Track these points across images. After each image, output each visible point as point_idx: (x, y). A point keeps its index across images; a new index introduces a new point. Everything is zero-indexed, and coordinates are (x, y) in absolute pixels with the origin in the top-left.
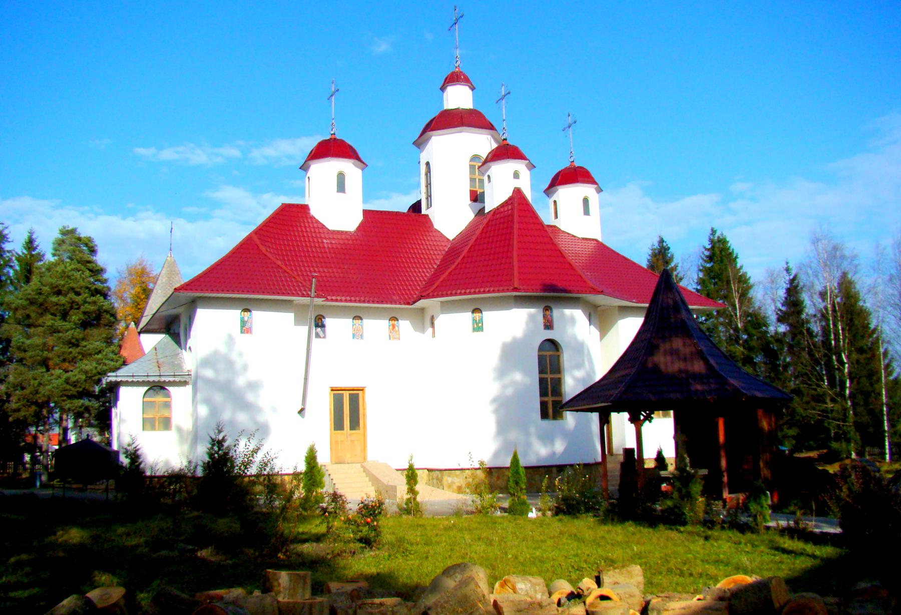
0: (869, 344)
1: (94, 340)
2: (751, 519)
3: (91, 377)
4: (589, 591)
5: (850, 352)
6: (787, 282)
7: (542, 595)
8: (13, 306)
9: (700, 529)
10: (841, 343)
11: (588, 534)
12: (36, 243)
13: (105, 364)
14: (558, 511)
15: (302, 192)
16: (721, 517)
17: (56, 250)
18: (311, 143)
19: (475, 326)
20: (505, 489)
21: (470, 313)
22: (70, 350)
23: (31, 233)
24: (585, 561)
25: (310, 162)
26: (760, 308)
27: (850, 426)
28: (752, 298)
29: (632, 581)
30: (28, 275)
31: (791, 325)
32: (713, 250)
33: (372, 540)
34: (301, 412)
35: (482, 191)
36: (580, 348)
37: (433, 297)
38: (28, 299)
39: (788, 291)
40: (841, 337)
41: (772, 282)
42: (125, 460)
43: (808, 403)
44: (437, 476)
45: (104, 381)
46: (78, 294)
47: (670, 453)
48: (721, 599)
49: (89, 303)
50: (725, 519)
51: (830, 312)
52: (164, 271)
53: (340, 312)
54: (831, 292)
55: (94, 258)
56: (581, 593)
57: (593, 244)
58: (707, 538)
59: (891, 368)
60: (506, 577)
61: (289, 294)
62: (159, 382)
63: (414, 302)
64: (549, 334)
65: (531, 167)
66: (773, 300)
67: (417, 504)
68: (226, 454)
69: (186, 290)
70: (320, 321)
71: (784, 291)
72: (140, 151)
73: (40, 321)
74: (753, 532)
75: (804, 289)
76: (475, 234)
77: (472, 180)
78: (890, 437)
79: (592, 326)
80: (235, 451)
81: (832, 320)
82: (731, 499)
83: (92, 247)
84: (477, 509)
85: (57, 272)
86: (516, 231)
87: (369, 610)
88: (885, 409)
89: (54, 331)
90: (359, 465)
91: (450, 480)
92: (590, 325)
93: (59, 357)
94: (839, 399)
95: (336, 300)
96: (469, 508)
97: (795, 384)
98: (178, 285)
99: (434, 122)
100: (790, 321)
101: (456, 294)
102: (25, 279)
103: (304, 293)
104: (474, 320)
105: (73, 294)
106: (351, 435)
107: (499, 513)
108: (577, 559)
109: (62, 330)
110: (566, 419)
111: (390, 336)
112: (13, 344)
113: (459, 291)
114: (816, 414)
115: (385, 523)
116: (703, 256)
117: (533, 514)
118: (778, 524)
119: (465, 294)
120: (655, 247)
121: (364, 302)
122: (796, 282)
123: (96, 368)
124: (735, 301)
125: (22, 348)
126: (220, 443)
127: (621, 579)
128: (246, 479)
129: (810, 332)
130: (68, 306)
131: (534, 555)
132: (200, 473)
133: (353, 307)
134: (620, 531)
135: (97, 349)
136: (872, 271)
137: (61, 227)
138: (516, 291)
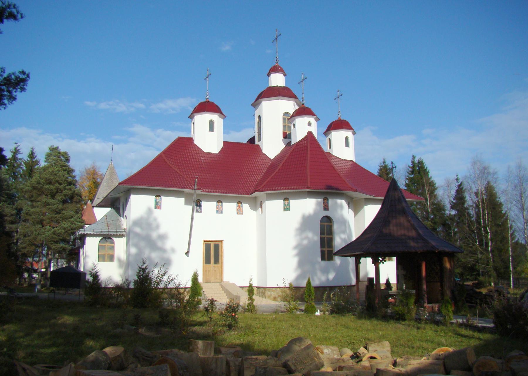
1: (69, 211)
2: (442, 318)
3: (67, 231)
4: (364, 354)
6: (457, 186)
7: (337, 356)
8: (24, 190)
9: (413, 323)
10: (487, 222)
11: (352, 325)
12: (35, 155)
13: (75, 225)
14: (332, 312)
15: (189, 130)
16: (426, 316)
17: (46, 158)
20: (302, 300)
21: (283, 200)
22: (56, 216)
24: (354, 339)
25: (195, 114)
27: (491, 268)
28: (436, 195)
29: (384, 349)
30: (31, 173)
31: (458, 210)
32: (414, 168)
33: (233, 325)
34: (187, 253)
35: (289, 132)
36: (344, 222)
37: (262, 191)
38: (33, 187)
39: (457, 191)
41: (448, 186)
42: (89, 277)
43: (467, 254)
45: (77, 233)
46: (60, 184)
47: (393, 281)
48: (437, 359)
50: (427, 318)
51: (481, 204)
52: (108, 172)
53: (209, 199)
54: (482, 192)
56: (359, 355)
57: (350, 163)
58: (418, 328)
60: (318, 346)
61: (182, 187)
62: (108, 234)
63: (251, 194)
64: (326, 213)
65: (317, 120)
66: (449, 197)
67: (254, 306)
68: (147, 276)
69: (125, 184)
70: (199, 203)
71: (455, 191)
72: (89, 103)
73: (39, 199)
74: (443, 325)
75: (466, 191)
76: (286, 156)
77: (284, 126)
78: (514, 274)
79: (350, 209)
80: (153, 274)
81: (482, 208)
82: (429, 307)
84: (287, 309)
85: (49, 171)
86: (309, 155)
87: (250, 362)
88: (511, 258)
89: (46, 204)
90: (219, 284)
91: (269, 293)
92: (349, 208)
93: (49, 219)
94: (485, 253)
95: (208, 192)
96: (283, 309)
97: (460, 243)
98: (121, 181)
99: (264, 93)
100: (458, 208)
101: (275, 190)
102: (29, 175)
103: (191, 187)
104: (285, 205)
105: (58, 184)
106: (214, 267)
107: (299, 312)
108: (349, 338)
109: (51, 204)
110: (335, 261)
111: (237, 212)
112: (24, 211)
113: (277, 188)
114: (472, 260)
115: (239, 316)
116: (408, 171)
117: (318, 314)
118: (457, 321)
119: (280, 189)
120: (382, 165)
121: (224, 193)
122: (462, 186)
123: (70, 226)
124: (427, 196)
127: (378, 348)
130: (55, 191)
131: (325, 336)
132: (132, 286)
133: (217, 195)
134: (369, 323)
135: (70, 215)
138: (309, 189)
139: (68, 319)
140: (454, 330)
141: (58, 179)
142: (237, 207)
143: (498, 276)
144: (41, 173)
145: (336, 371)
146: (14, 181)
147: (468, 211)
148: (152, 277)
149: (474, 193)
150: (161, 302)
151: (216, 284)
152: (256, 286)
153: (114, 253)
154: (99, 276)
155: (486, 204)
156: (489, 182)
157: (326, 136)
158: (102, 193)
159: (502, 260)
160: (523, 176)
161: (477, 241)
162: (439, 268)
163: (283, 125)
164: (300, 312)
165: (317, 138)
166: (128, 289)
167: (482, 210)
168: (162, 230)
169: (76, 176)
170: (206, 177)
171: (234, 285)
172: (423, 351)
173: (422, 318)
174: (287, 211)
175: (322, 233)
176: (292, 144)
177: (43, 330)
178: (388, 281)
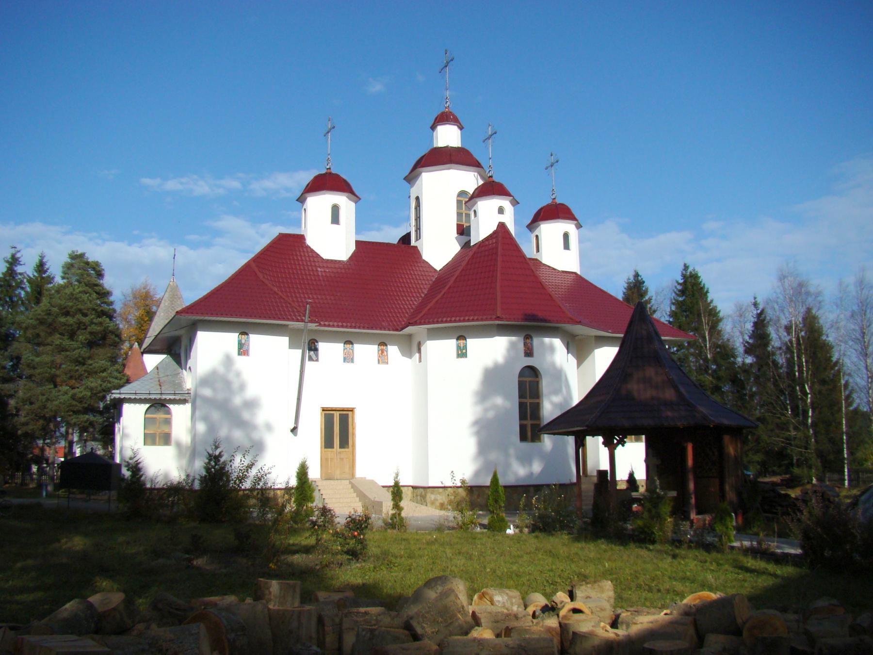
0: (831, 376)
1: (100, 360)
2: (716, 539)
3: (96, 394)
4: (563, 604)
5: (813, 383)
7: (518, 607)
8: (24, 325)
10: (805, 375)
11: (563, 551)
12: (47, 267)
13: (110, 382)
14: (534, 529)
15: (298, 223)
16: (689, 536)
17: (65, 273)
18: (308, 177)
19: (460, 352)
20: (484, 507)
22: (77, 368)
23: (42, 257)
24: (560, 576)
25: (307, 195)
26: (728, 340)
27: (812, 453)
29: (603, 595)
30: (39, 296)
31: (757, 357)
32: (686, 285)
33: (359, 552)
34: (294, 430)
35: (468, 225)
36: (559, 375)
37: (420, 324)
38: (38, 319)
40: (805, 369)
41: (741, 316)
42: (126, 473)
44: (422, 493)
45: (108, 398)
46: (85, 315)
47: (641, 475)
49: (96, 324)
50: (692, 538)
51: (795, 345)
53: (332, 337)
54: (796, 326)
55: (101, 281)
56: (555, 606)
57: (572, 277)
58: (674, 556)
59: (851, 399)
62: (160, 399)
63: (402, 329)
64: (529, 362)
65: (515, 203)
66: (742, 333)
67: (402, 519)
68: (223, 468)
69: (187, 313)
70: (313, 345)
72: (147, 181)
73: (49, 340)
74: (718, 552)
75: (771, 323)
77: (459, 215)
78: (849, 464)
79: (570, 355)
80: (231, 466)
82: (698, 520)
83: (99, 271)
84: (458, 524)
86: (499, 263)
87: (355, 618)
88: (845, 437)
89: (61, 349)
90: (348, 481)
91: (433, 497)
92: (568, 353)
93: (66, 374)
95: (329, 326)
96: (451, 524)
97: (760, 412)
98: (179, 309)
99: (424, 159)
100: (757, 353)
101: (442, 322)
103: (299, 318)
104: (459, 347)
105: (80, 315)
106: (340, 453)
108: (551, 574)
116: (675, 290)
117: (510, 531)
118: (742, 544)
119: (451, 322)
120: (631, 281)
125: (32, 365)
126: (217, 458)
127: (593, 594)
128: (241, 493)
129: (775, 363)
130: (75, 327)
131: (511, 570)
132: (197, 486)
134: (592, 548)
135: (102, 367)
136: (835, 307)
137: (70, 252)
139: (78, 543)
140: (735, 560)
141: (80, 306)
142: (378, 351)
143: (824, 467)
144: (52, 297)
145: (501, 637)
146: (10, 310)
147: (774, 358)
148: (230, 471)
149: (783, 328)
150: (246, 512)
151: (343, 481)
152: (411, 484)
153: (171, 431)
154: (141, 469)
155: (803, 347)
156: (809, 310)
157: (531, 231)
158: (156, 327)
159: (832, 441)
160: (867, 298)
161: (789, 407)
162: (716, 453)
163: (457, 213)
164: (480, 528)
165: (513, 235)
166: (192, 491)
167: (798, 357)
168: (250, 393)
169: (114, 301)
170: (325, 301)
171: (372, 483)
172: (674, 597)
173: (682, 539)
174: (463, 359)
175: (521, 395)
176: (472, 244)
177: (30, 562)
178: (631, 475)
